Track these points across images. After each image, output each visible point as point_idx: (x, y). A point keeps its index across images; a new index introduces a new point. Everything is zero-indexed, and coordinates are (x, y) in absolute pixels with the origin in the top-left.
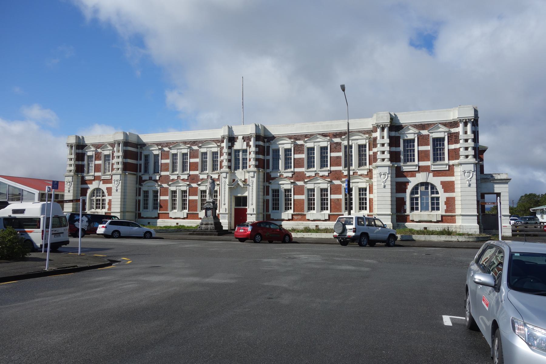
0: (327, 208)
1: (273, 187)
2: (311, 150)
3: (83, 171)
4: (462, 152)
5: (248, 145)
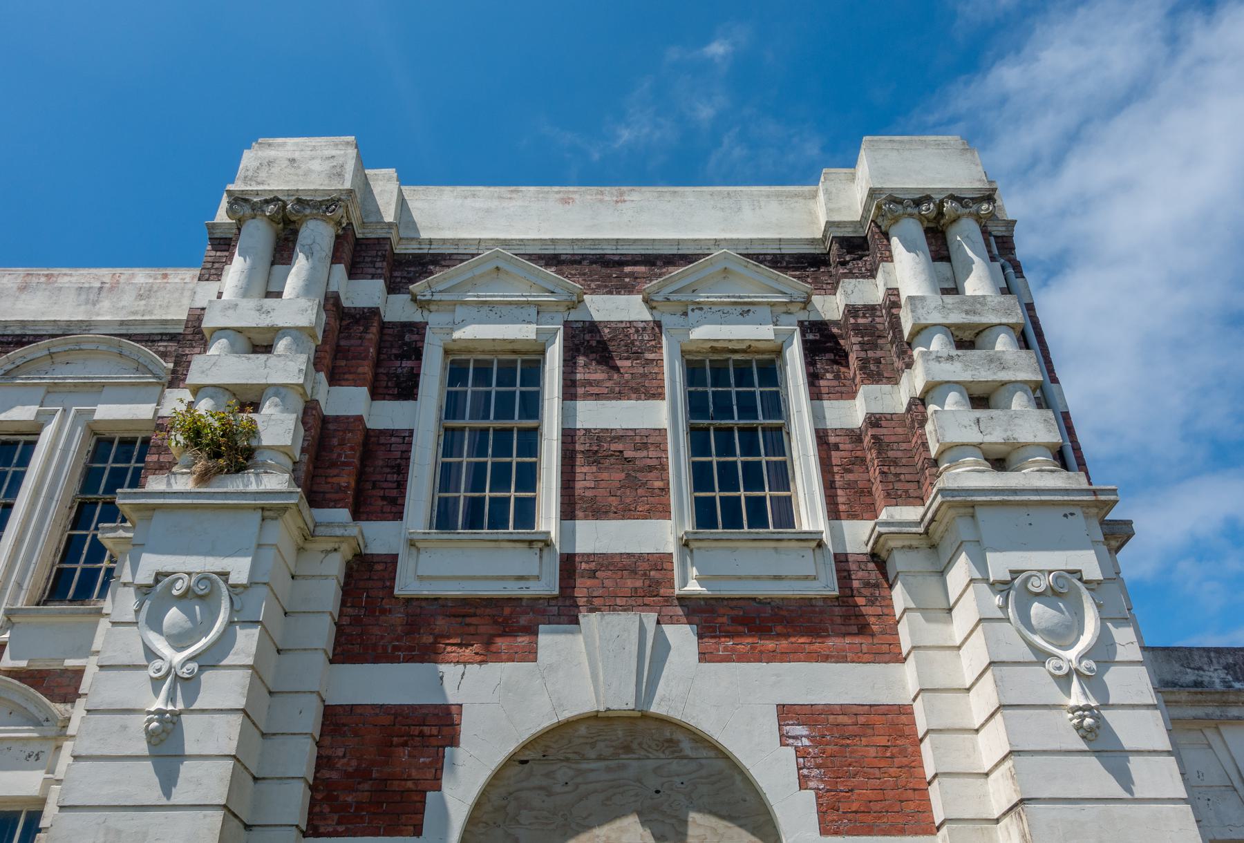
4: (951, 422)
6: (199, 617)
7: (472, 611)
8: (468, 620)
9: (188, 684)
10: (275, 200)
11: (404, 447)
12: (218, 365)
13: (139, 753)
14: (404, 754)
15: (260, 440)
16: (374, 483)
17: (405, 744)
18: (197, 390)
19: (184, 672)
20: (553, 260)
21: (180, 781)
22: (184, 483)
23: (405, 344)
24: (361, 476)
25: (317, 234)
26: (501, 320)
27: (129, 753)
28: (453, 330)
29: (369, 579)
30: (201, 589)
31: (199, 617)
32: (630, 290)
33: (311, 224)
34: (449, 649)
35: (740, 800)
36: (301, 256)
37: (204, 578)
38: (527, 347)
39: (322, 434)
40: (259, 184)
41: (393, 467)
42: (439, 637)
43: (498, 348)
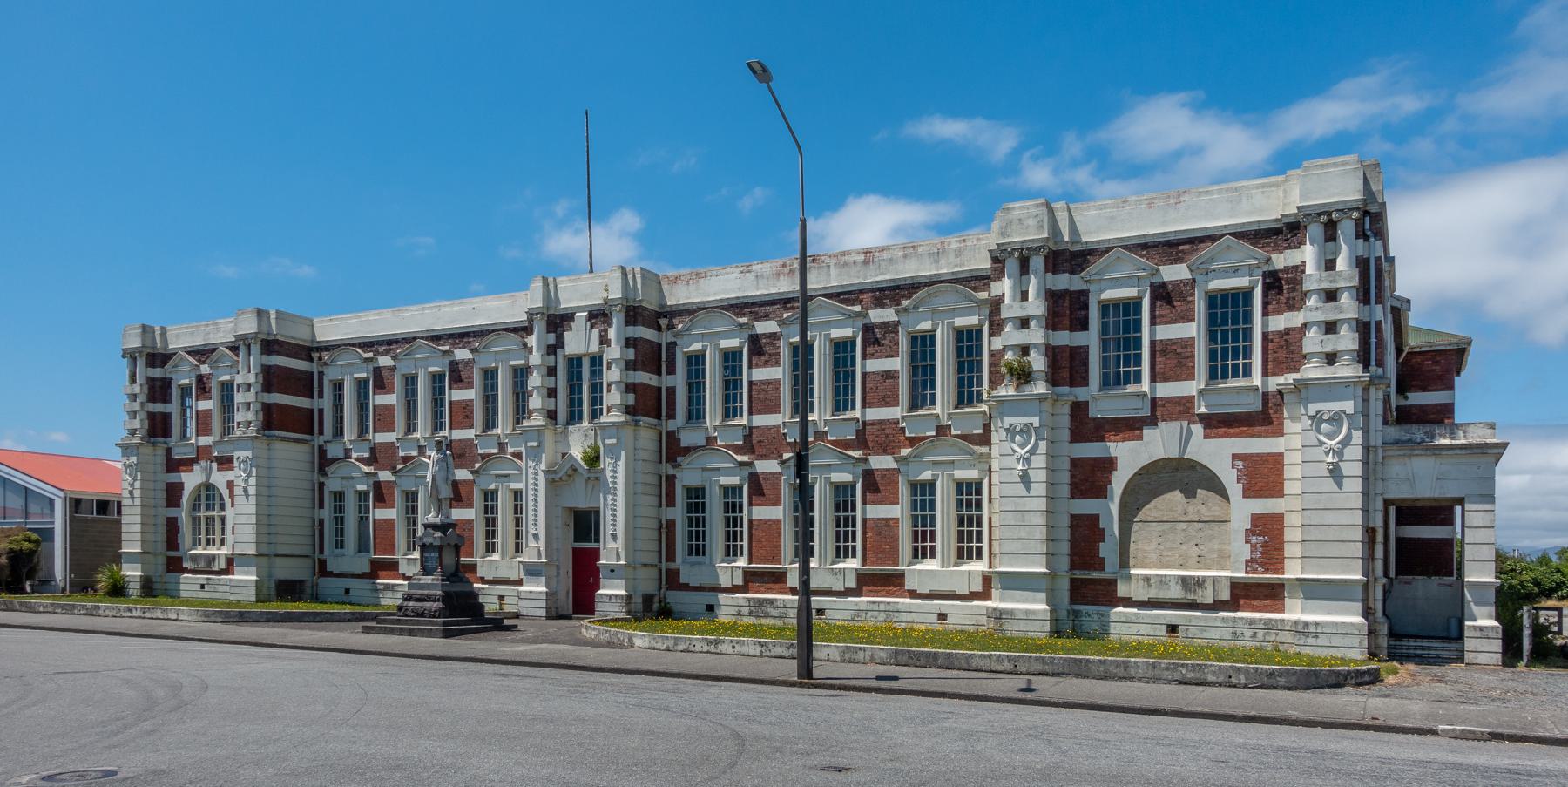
0: (979, 550)
1: (333, 484)
2: (923, 345)
3: (166, 433)
4: (1313, 341)
5: (604, 340)
20: (1145, 246)
22: (1011, 391)
24: (1071, 368)
25: (1038, 262)
32: (1180, 260)
35: (1215, 485)
39: (1053, 353)
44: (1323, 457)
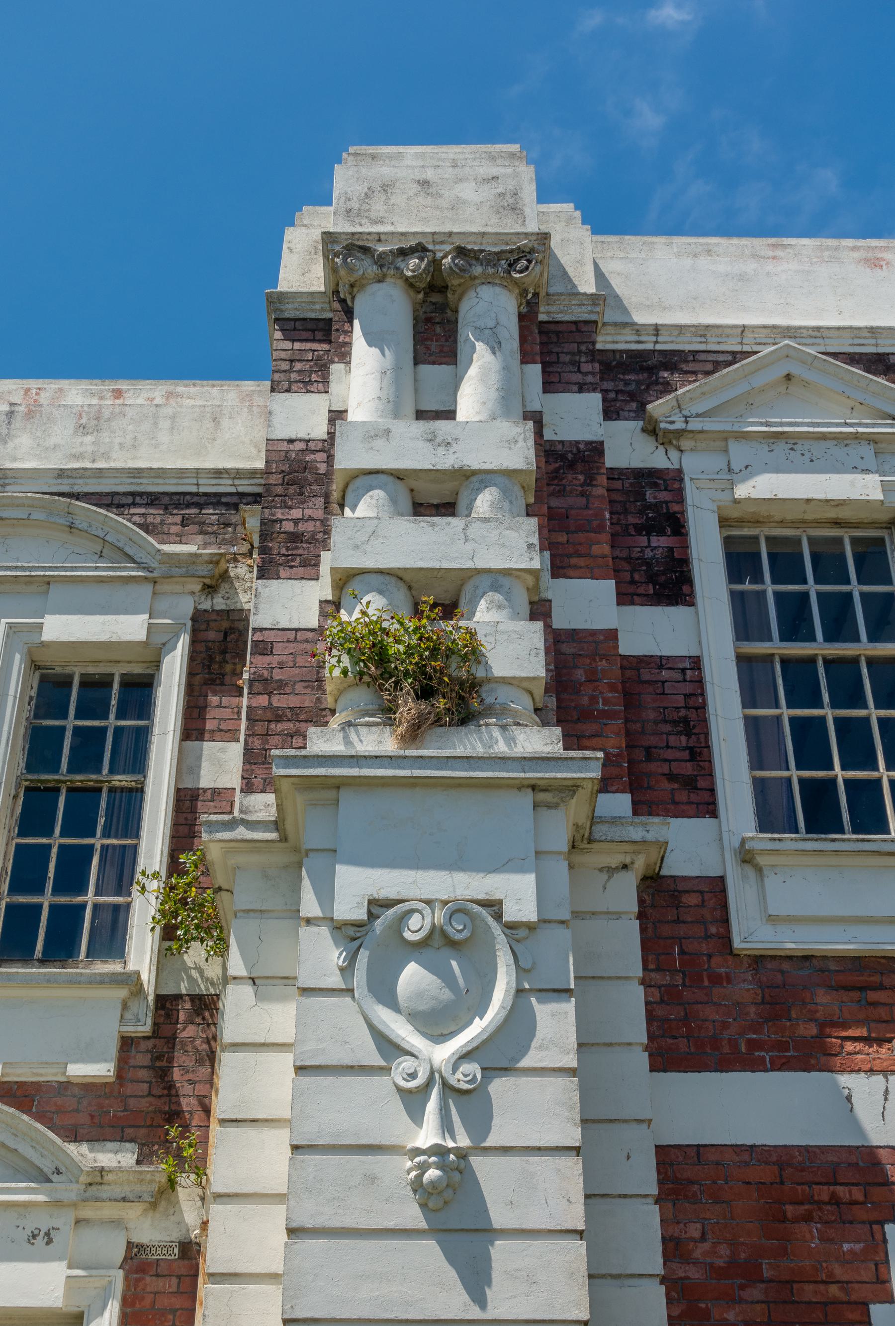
6: (461, 981)
7: (876, 978)
8: (873, 996)
9: (468, 1102)
10: (420, 249)
11: (688, 688)
12: (372, 534)
13: (409, 1226)
14: (811, 1235)
15: (487, 667)
16: (648, 750)
17: (807, 1218)
18: (346, 580)
19: (459, 1080)
21: (496, 1275)
23: (650, 507)
25: (491, 308)
26: (812, 466)
27: (391, 1224)
28: (732, 485)
29: (678, 921)
30: (458, 929)
31: (461, 981)
33: (486, 293)
34: (849, 1046)
36: (480, 346)
37: (458, 909)
38: (864, 515)
40: (375, 222)
41: (675, 723)
42: (826, 1025)
43: (809, 516)
44: (393, 1124)
